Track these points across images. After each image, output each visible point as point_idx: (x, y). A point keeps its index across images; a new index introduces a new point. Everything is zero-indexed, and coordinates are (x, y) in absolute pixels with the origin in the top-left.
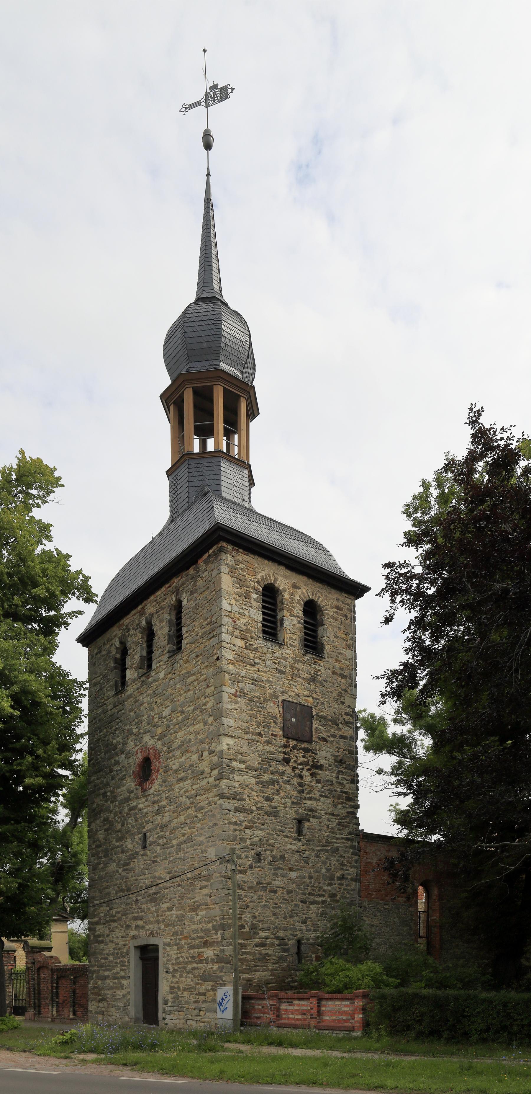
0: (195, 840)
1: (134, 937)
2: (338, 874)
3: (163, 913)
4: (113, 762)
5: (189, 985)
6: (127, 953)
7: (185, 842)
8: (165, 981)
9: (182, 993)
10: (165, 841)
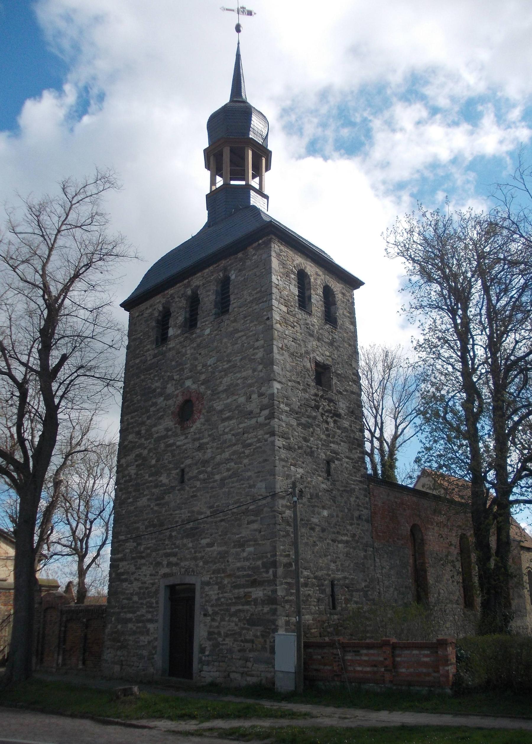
0: (241, 475)
1: (165, 575)
2: (356, 514)
3: (202, 550)
4: (150, 403)
5: (233, 630)
6: (157, 592)
7: (230, 477)
8: (202, 625)
9: (224, 640)
10: (206, 476)
